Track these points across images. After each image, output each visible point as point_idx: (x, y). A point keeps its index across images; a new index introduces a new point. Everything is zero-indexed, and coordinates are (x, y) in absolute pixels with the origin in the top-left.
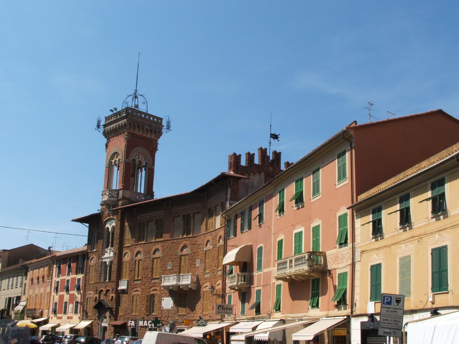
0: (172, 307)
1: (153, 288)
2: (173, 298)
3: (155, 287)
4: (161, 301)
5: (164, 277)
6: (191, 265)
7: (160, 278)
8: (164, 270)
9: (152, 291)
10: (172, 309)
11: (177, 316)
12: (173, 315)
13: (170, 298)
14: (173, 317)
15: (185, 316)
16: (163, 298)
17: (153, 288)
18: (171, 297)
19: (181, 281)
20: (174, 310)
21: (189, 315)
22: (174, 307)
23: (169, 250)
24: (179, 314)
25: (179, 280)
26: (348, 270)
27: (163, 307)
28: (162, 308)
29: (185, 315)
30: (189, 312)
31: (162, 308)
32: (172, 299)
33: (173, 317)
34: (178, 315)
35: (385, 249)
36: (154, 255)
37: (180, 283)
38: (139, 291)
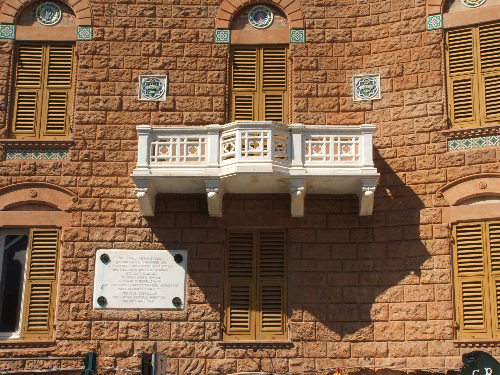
0: (177, 301)
1: (23, 195)
2: (184, 254)
3: (37, 190)
4: (88, 270)
5: (153, 136)
6: (309, 95)
7: (73, 144)
8: (113, 102)
9: (459, 203)
10: (182, 314)
11: (215, 348)
12: (190, 345)
13: (166, 256)
14: (190, 355)
15: (284, 352)
16: (100, 253)
17: (23, 195)
18: (168, 246)
19: (297, 160)
20: (193, 315)
21: (311, 348)
22: (190, 302)
23: (142, 15)
24: (228, 340)
25: (283, 152)
26: (488, 223)
27: (102, 301)
28: (96, 305)
29: (288, 346)
30: (315, 328)
31: (96, 305)
32: (178, 259)
33: (190, 355)
34: (225, 346)
35: (220, 175)
36: (445, 15)
37: (294, 171)
38: (53, 207)
